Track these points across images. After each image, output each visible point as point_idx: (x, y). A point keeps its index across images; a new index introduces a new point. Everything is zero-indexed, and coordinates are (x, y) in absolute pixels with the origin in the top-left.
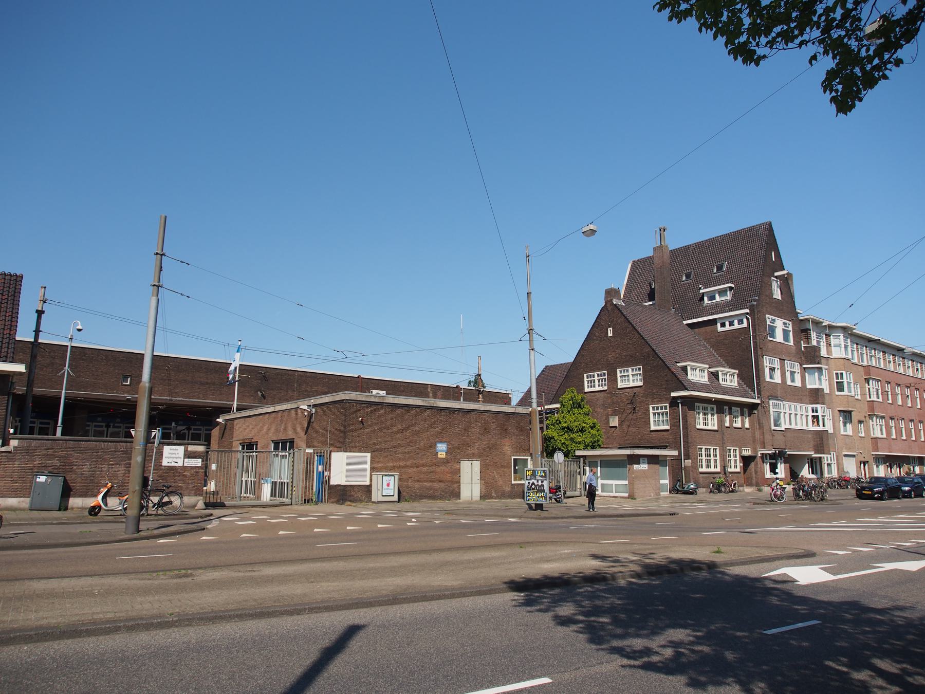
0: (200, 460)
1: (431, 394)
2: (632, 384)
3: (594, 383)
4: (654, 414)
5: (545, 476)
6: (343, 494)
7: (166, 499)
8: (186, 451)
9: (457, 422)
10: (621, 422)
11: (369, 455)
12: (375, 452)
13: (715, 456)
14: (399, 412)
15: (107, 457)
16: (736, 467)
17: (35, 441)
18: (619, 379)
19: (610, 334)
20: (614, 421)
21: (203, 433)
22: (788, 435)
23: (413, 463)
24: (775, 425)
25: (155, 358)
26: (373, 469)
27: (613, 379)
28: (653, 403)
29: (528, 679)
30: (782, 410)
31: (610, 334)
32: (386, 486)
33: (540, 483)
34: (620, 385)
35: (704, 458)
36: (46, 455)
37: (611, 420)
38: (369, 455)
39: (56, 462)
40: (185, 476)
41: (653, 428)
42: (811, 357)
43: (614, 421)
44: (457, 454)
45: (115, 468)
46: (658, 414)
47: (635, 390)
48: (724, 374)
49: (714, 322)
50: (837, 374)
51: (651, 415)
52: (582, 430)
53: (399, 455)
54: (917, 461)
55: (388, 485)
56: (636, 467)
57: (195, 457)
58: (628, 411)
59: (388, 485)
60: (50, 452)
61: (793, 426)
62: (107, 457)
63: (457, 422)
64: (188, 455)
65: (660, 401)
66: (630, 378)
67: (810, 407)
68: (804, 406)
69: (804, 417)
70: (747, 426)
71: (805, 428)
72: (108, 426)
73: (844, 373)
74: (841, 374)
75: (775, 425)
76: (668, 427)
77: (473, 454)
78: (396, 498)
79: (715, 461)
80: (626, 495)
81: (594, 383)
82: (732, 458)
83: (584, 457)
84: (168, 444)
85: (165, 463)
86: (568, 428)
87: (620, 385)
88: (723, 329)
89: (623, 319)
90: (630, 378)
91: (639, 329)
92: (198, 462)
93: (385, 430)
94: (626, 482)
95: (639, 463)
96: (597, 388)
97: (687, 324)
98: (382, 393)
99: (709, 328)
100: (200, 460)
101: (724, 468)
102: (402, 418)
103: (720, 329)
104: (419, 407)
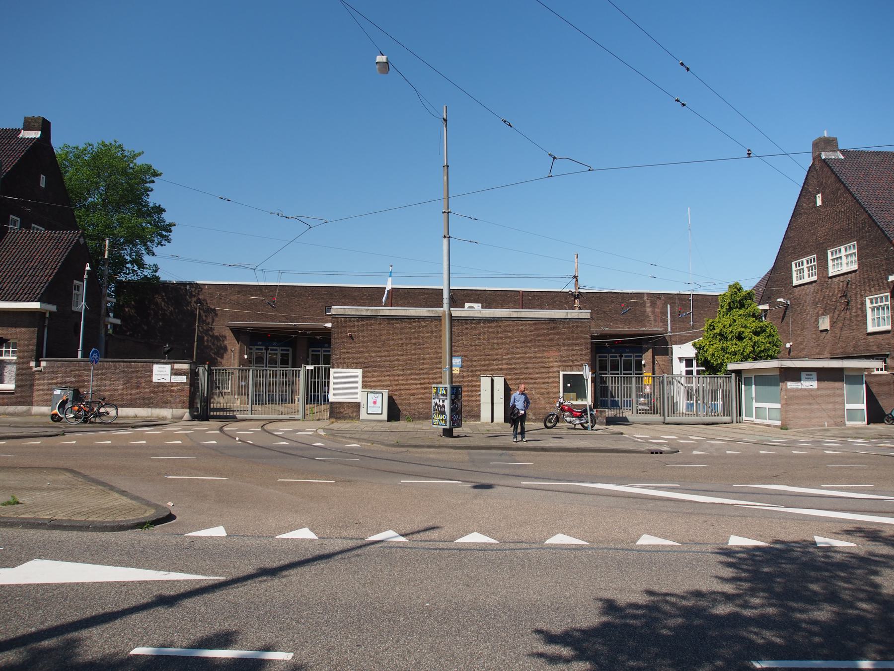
0: (185, 377)
2: (845, 269)
3: (803, 273)
4: (873, 309)
5: (446, 395)
6: (339, 411)
7: (102, 410)
8: (172, 369)
9: (476, 333)
10: (833, 324)
11: (360, 371)
12: (366, 367)
14: (396, 324)
15: (109, 374)
17: (60, 362)
18: (830, 263)
19: (819, 203)
20: (825, 323)
21: (633, 359)
23: (415, 379)
25: (450, 290)
26: (365, 386)
27: (823, 264)
28: (871, 293)
31: (819, 203)
32: (375, 405)
33: (441, 403)
34: (832, 271)
36: (65, 373)
37: (821, 321)
38: (360, 371)
39: (72, 379)
40: (172, 391)
41: (870, 329)
43: (825, 323)
44: (473, 370)
45: (116, 384)
46: (878, 308)
47: (849, 277)
51: (869, 311)
52: (740, 337)
53: (399, 371)
55: (375, 403)
56: (791, 385)
57: (181, 375)
58: (840, 308)
59: (375, 403)
60: (68, 370)
62: (109, 374)
63: (476, 333)
64: (175, 373)
66: (844, 261)
72: (267, 349)
76: (888, 327)
77: (501, 370)
78: (385, 416)
80: (779, 423)
83: (738, 372)
84: (157, 363)
85: (155, 379)
86: (720, 334)
87: (832, 271)
89: (833, 178)
91: (853, 189)
92: (183, 379)
93: (380, 345)
94: (778, 406)
95: (799, 380)
96: (807, 280)
98: (477, 306)
100: (185, 377)
102: (402, 330)
104: (423, 318)
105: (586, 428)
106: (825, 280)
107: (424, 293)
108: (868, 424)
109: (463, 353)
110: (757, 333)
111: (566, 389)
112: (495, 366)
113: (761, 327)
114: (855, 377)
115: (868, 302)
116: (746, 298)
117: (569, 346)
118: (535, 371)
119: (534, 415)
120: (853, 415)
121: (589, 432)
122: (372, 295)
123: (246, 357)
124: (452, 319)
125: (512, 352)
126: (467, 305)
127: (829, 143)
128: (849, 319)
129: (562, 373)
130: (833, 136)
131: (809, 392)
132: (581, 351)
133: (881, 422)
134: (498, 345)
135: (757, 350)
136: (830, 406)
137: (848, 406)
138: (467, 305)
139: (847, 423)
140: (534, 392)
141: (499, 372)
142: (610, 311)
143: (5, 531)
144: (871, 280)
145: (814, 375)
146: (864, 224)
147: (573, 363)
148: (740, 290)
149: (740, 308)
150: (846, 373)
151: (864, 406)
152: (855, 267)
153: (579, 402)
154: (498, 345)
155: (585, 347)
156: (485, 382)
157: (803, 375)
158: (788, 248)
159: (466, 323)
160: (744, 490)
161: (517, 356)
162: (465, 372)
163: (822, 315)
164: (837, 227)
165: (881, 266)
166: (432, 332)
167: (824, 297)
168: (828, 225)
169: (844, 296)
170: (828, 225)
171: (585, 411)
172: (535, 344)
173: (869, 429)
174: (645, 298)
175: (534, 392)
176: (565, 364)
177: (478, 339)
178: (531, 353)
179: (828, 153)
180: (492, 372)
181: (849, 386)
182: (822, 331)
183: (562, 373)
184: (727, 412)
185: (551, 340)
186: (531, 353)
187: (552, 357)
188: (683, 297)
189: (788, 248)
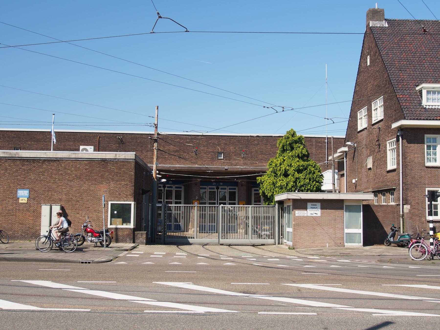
9: (41, 170)
52: (286, 175)
56: (299, 213)
63: (41, 170)
89: (374, 44)
95: (306, 208)
98: (90, 149)
105: (102, 246)
107: (180, 138)
108: (365, 244)
109: (30, 186)
110: (299, 171)
111: (113, 216)
112: (56, 196)
113: (303, 166)
114: (351, 206)
115: (388, 145)
116: (296, 142)
117: (117, 181)
118: (88, 201)
120: (351, 237)
121: (104, 249)
122: (39, 139)
123: (116, 212)
125: (71, 186)
126: (81, 147)
127: (375, 14)
129: (110, 203)
130: (381, 8)
131: (315, 218)
132: (127, 185)
133: (381, 242)
134: (59, 180)
135: (299, 185)
136: (331, 230)
137: (346, 231)
138: (81, 147)
139: (346, 244)
141: (55, 202)
142: (257, 151)
145: (319, 205)
147: (120, 194)
148: (293, 135)
149: (292, 151)
150: (345, 204)
151: (361, 231)
153: (125, 226)
154: (59, 180)
155: (130, 181)
156: (45, 209)
157: (309, 205)
159: (34, 163)
161: (74, 189)
162: (32, 202)
166: (6, 169)
169: (378, 140)
171: (102, 233)
172: (89, 179)
173: (367, 251)
176: (112, 195)
178: (85, 187)
179: (375, 22)
180: (51, 202)
181: (347, 213)
183: (110, 203)
184: (272, 236)
185: (102, 176)
186: (85, 187)
187: (103, 190)
188: (320, 140)
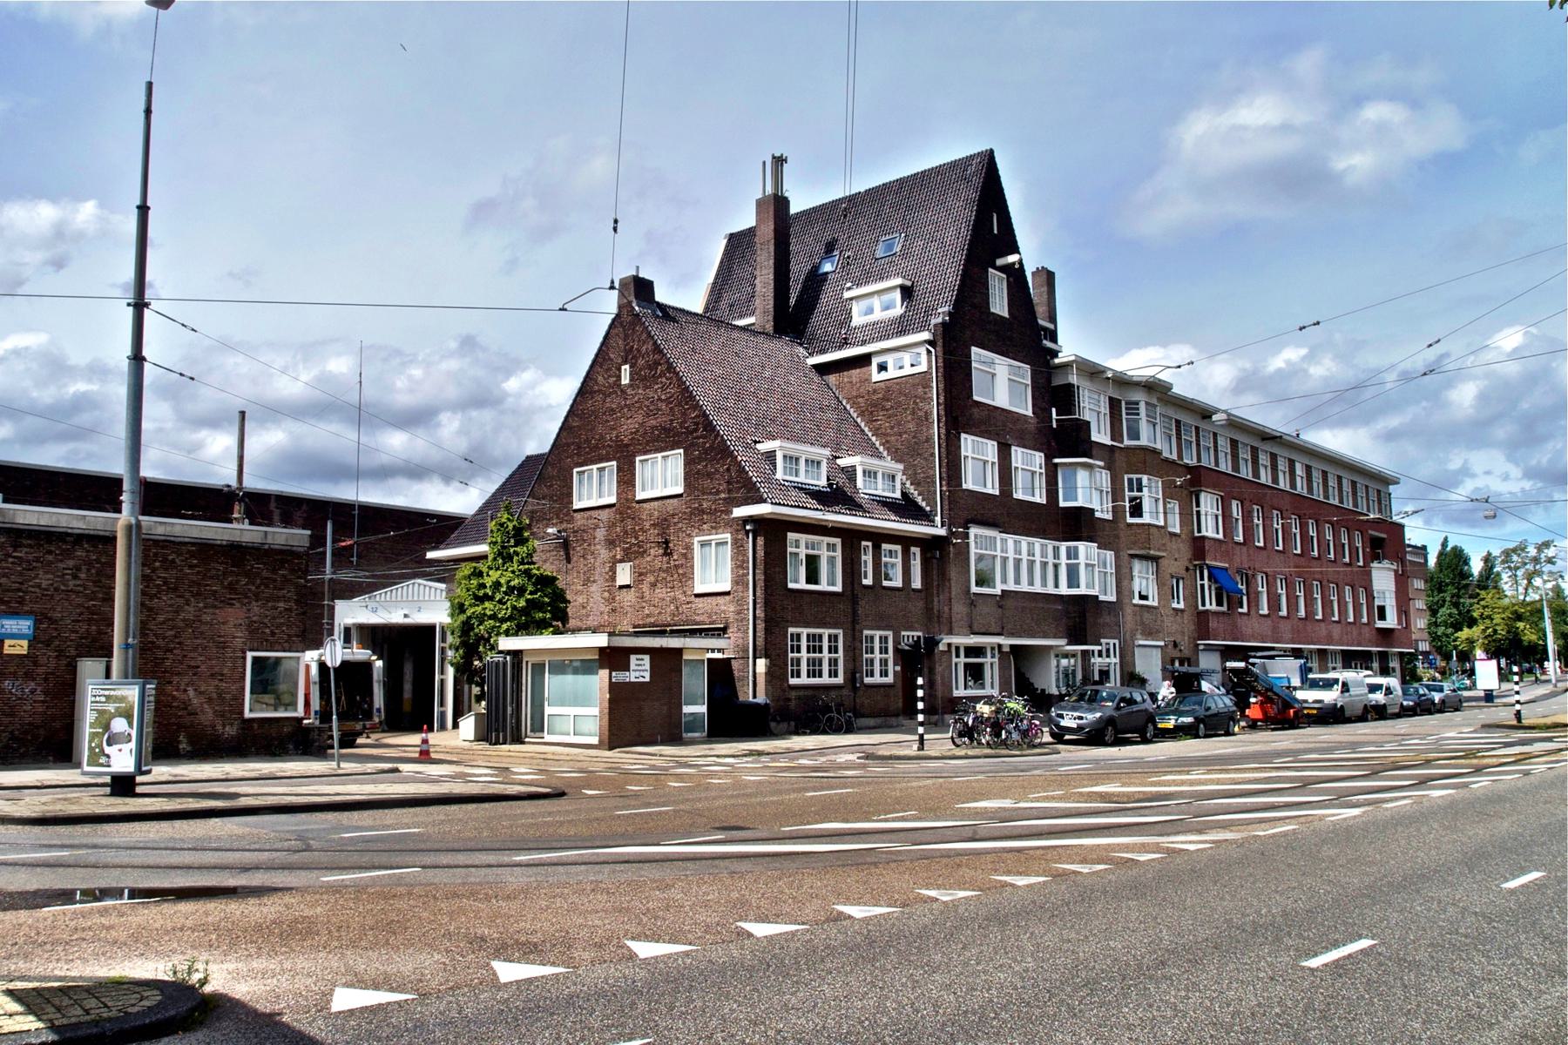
1: (276, 517)
3: (593, 489)
9: (71, 563)
10: (639, 575)
13: (884, 650)
16: (884, 673)
19: (625, 380)
22: (1009, 603)
24: (979, 583)
27: (626, 480)
28: (701, 532)
29: (1327, 950)
30: (998, 553)
31: (625, 380)
35: (804, 654)
42: (1064, 440)
48: (870, 474)
49: (864, 360)
50: (1130, 480)
54: (1339, 658)
61: (1024, 587)
63: (71, 563)
65: (715, 529)
66: (662, 475)
67: (1063, 546)
68: (1050, 544)
69: (1050, 569)
70: (917, 583)
71: (1051, 590)
73: (1145, 479)
74: (1139, 481)
75: (979, 583)
79: (884, 662)
81: (593, 489)
82: (877, 655)
88: (884, 376)
90: (662, 475)
97: (814, 366)
99: (855, 373)
101: (853, 675)
103: (876, 376)
106: (626, 506)
118: (195, 649)
119: (191, 743)
124: (994, 557)
128: (667, 571)
132: (289, 610)
140: (191, 693)
143: (10, 917)
144: (703, 512)
146: (697, 424)
152: (680, 490)
158: (568, 445)
159: (49, 542)
160: (592, 859)
161: (161, 618)
163: (621, 561)
164: (654, 422)
165: (718, 492)
167: (626, 533)
168: (640, 418)
170: (640, 418)
174: (273, 505)
175: (191, 693)
177: (75, 577)
178: (189, 612)
182: (621, 587)
183: (250, 655)
185: (231, 588)
189: (568, 445)
